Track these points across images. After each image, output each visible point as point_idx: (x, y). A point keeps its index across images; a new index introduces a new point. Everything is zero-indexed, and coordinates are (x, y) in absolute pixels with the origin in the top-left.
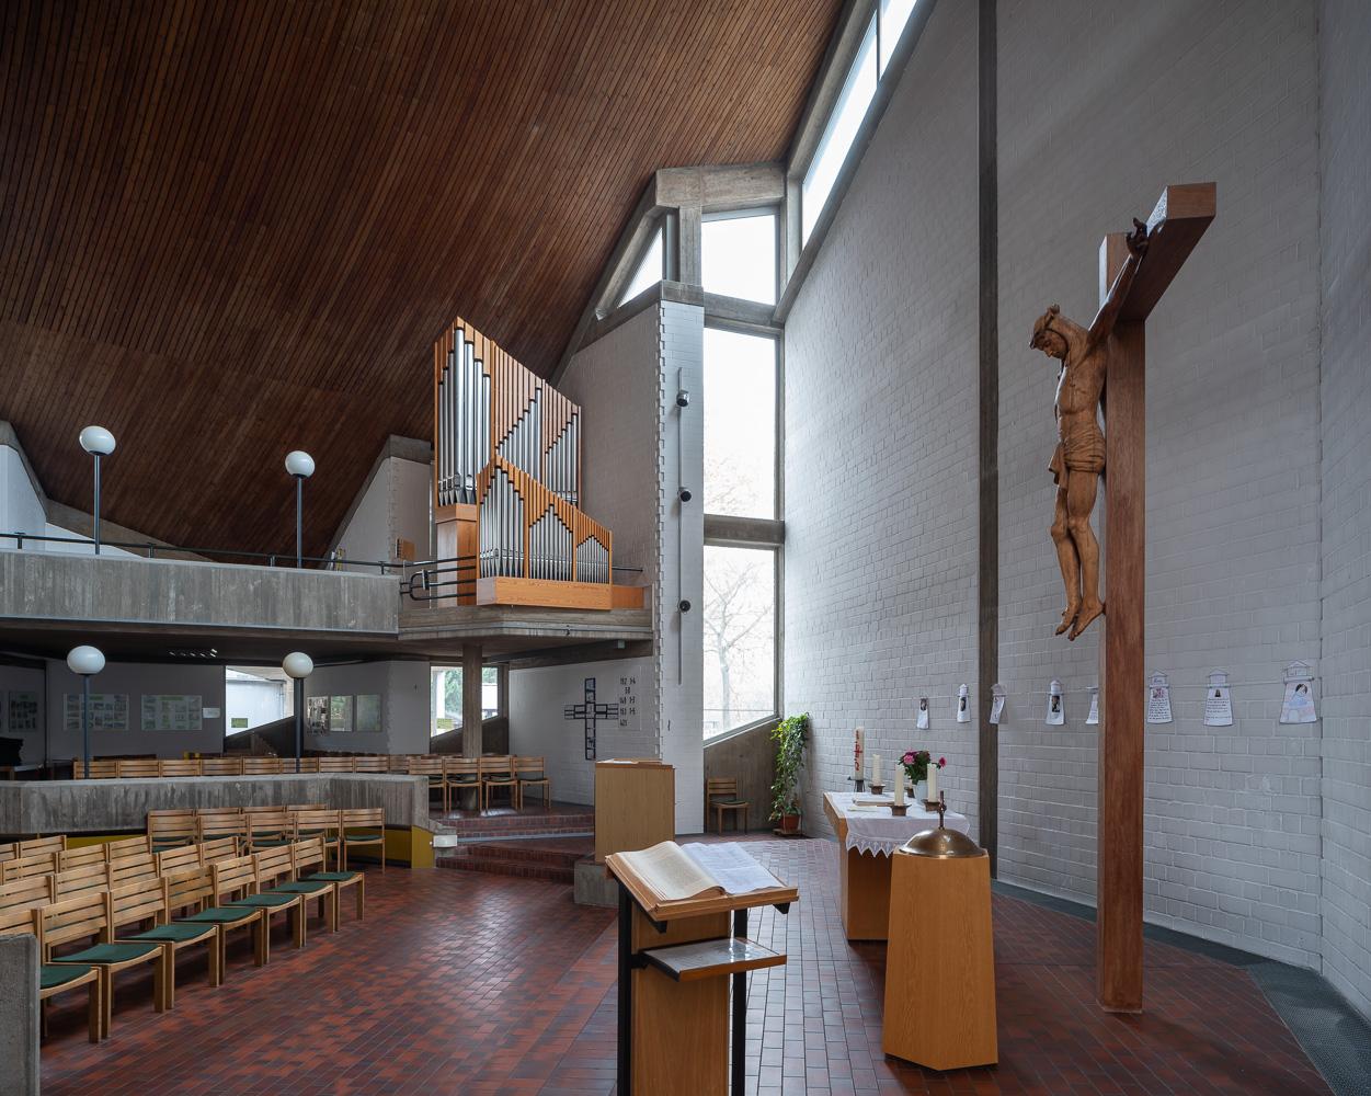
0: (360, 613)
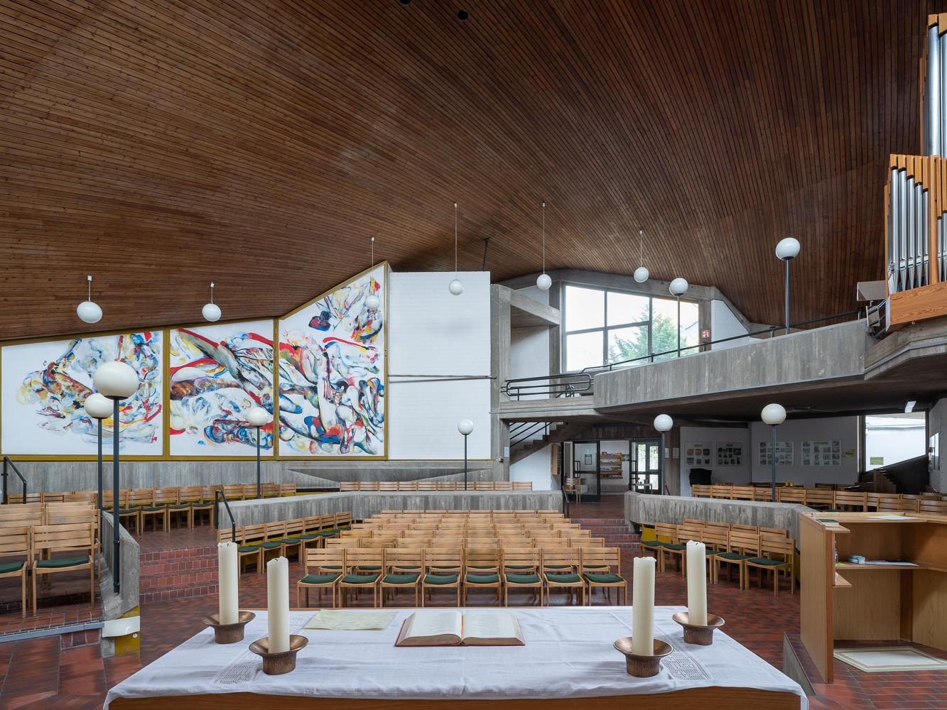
0: (829, 362)
